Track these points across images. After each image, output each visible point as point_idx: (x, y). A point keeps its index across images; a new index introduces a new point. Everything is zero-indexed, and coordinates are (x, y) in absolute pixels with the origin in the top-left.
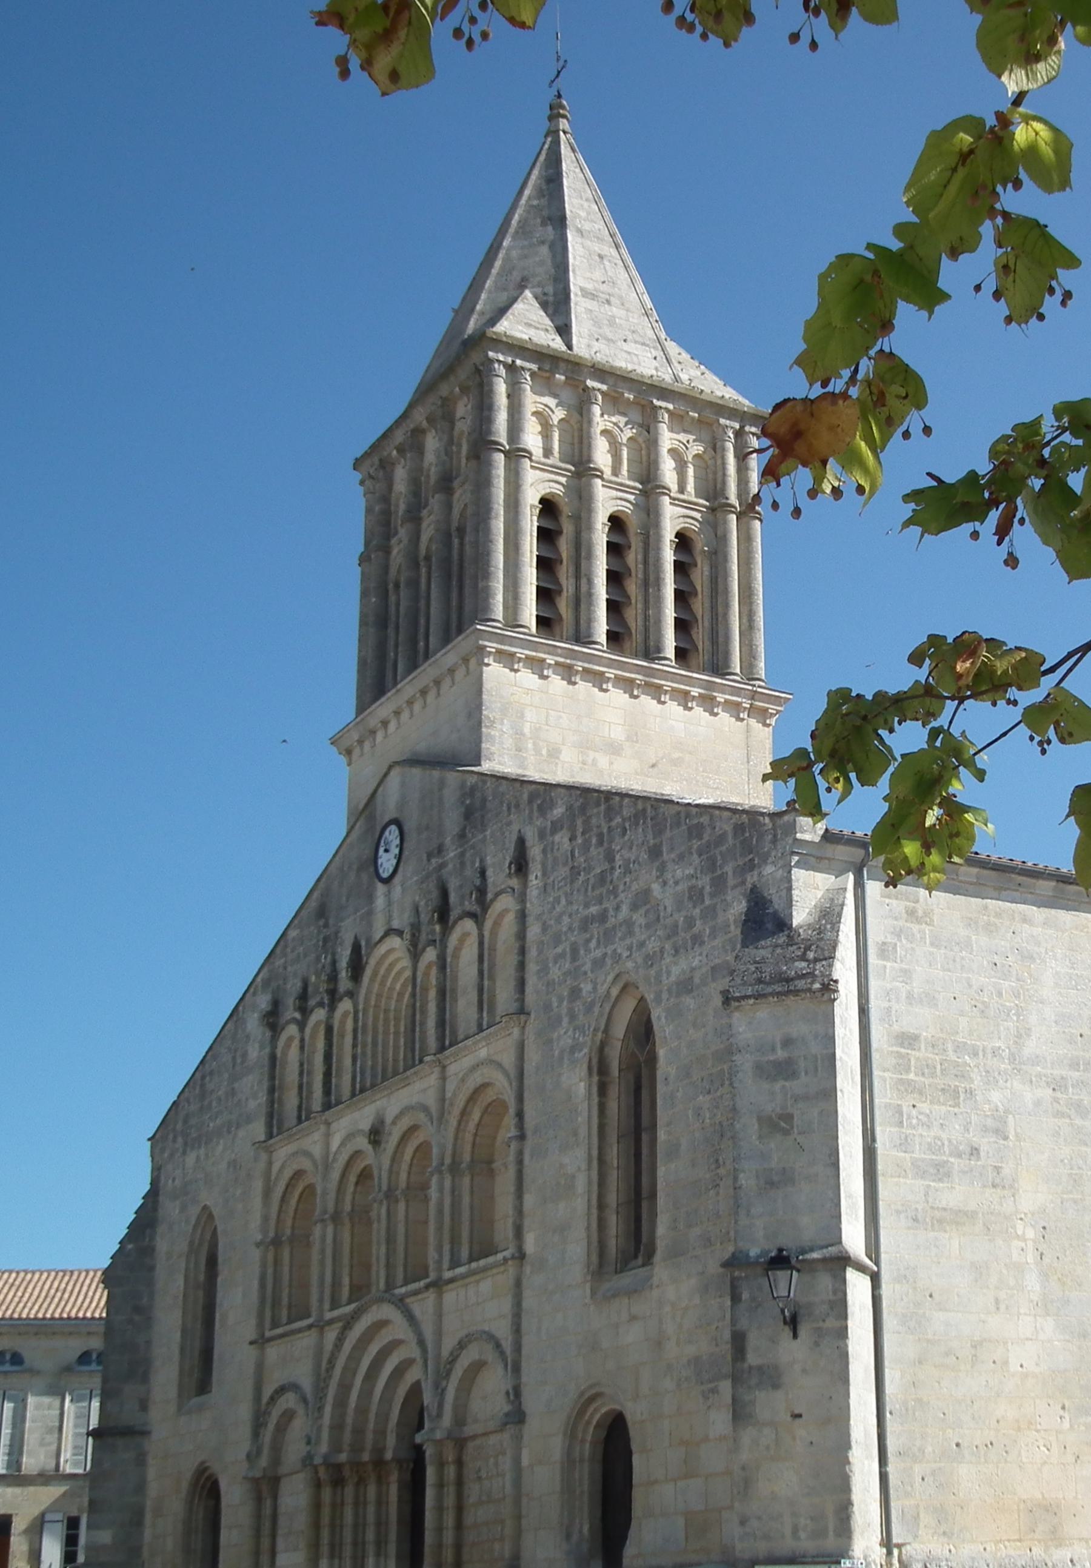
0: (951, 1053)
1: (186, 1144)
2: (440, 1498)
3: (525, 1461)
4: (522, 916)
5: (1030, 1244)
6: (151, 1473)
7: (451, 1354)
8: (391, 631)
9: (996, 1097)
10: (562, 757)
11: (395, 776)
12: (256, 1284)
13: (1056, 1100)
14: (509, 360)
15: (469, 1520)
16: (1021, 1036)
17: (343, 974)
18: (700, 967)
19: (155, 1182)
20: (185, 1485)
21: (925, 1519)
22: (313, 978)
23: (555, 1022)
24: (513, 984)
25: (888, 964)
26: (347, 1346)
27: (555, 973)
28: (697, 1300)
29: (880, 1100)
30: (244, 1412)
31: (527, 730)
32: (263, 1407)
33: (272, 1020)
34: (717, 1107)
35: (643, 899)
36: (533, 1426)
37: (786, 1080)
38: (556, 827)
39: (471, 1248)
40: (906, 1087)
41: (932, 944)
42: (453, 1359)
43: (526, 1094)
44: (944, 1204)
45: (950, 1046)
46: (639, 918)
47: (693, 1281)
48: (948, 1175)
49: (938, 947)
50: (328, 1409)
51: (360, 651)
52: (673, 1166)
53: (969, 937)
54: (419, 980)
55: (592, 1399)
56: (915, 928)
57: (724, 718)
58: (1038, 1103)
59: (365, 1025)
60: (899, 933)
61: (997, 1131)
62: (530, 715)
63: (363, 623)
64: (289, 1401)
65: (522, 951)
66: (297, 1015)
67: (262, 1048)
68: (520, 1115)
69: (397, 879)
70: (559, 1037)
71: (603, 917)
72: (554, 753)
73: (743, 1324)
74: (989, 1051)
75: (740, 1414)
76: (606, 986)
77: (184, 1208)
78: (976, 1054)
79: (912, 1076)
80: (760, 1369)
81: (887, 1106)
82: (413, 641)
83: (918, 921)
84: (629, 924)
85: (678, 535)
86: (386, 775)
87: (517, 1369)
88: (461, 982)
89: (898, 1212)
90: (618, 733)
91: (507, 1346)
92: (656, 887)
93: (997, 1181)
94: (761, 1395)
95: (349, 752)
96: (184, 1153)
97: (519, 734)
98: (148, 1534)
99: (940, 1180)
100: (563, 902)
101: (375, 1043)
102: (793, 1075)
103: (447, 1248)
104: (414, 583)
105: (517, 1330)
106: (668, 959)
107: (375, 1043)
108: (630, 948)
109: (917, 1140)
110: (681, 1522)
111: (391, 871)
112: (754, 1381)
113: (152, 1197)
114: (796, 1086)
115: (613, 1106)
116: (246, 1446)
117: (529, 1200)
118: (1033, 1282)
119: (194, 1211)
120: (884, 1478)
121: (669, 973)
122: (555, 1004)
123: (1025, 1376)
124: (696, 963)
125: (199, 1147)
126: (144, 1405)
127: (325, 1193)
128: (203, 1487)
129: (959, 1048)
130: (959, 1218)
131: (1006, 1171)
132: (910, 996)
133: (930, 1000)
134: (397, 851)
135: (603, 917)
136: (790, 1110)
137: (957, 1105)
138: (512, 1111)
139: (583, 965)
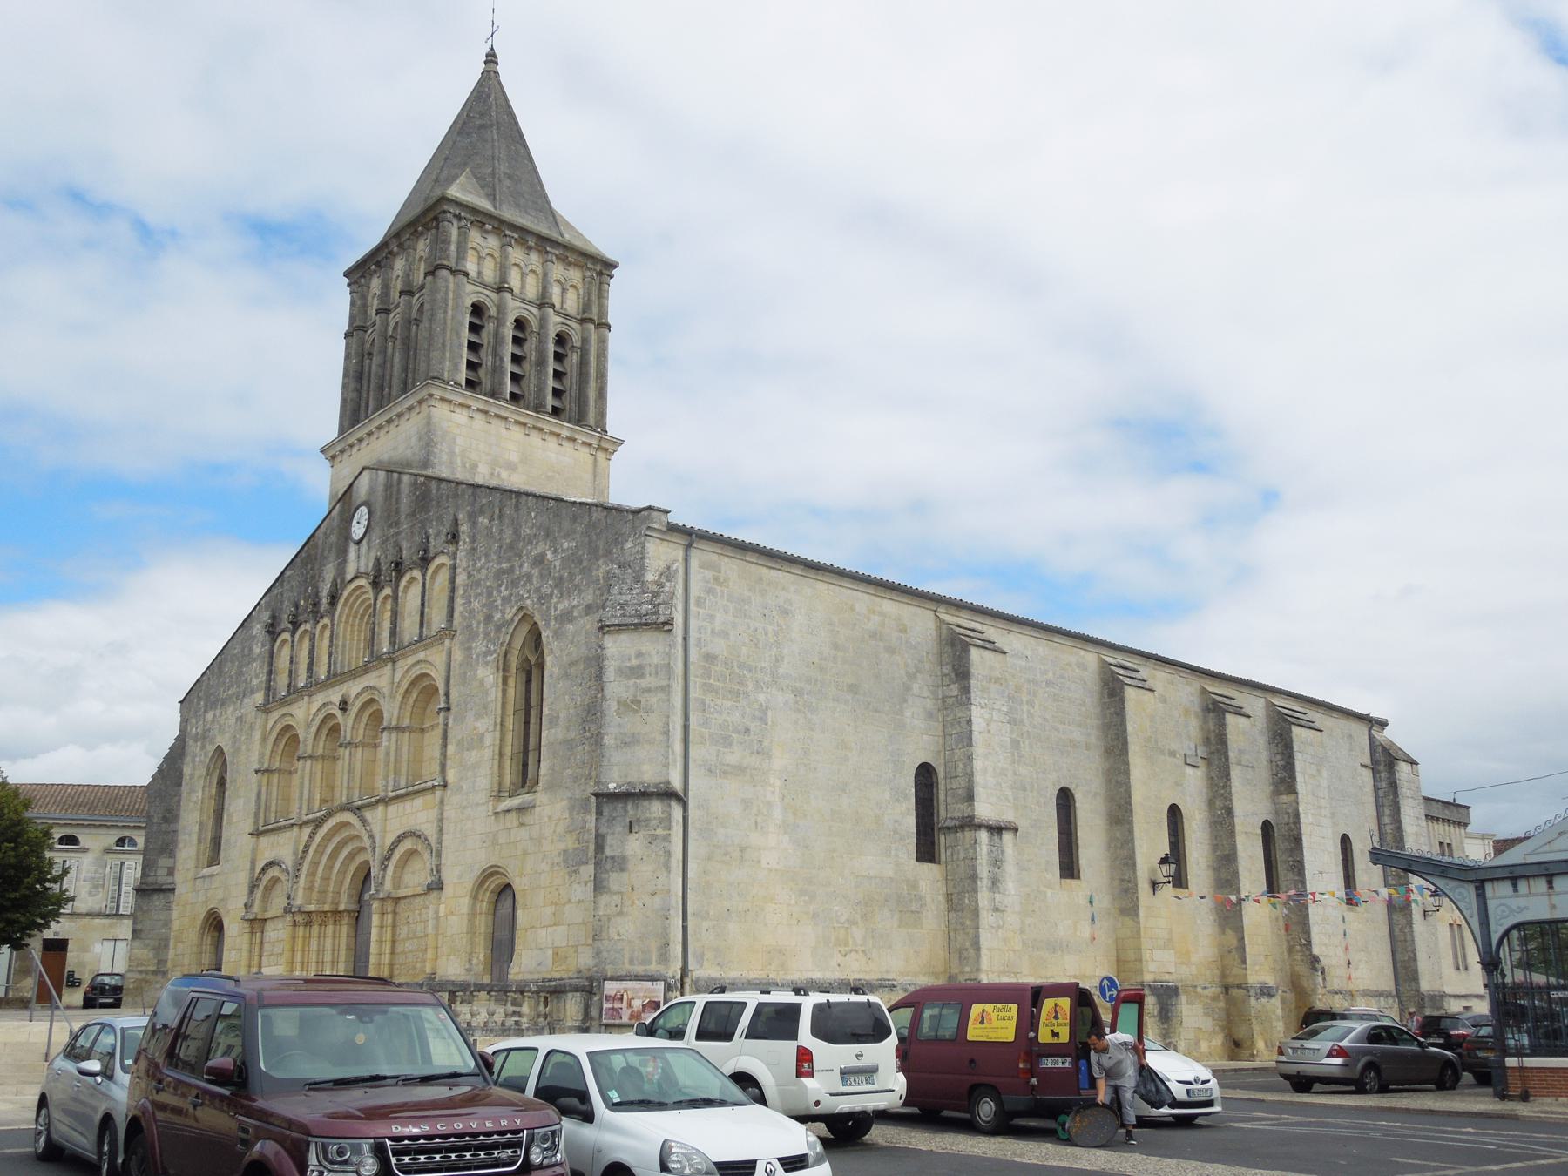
0: (736, 667)
1: (206, 706)
2: (380, 935)
3: (441, 914)
4: (454, 568)
5: (777, 789)
6: (175, 915)
7: (392, 844)
8: (365, 382)
9: (762, 697)
10: (479, 470)
11: (366, 476)
12: (254, 797)
13: (797, 702)
14: (457, 212)
15: (399, 948)
16: (778, 660)
17: (324, 601)
18: (578, 606)
19: (183, 731)
20: (199, 923)
21: (709, 955)
22: (302, 603)
23: (472, 636)
24: (445, 611)
25: (701, 611)
26: (318, 838)
27: (476, 605)
28: (566, 815)
29: (692, 695)
30: (243, 879)
31: (457, 451)
32: (256, 875)
33: (272, 631)
34: (586, 695)
35: (540, 560)
36: (448, 890)
37: (637, 678)
38: (482, 512)
39: (407, 779)
40: (708, 688)
41: (728, 600)
42: (392, 849)
43: (452, 682)
44: (727, 762)
45: (735, 664)
46: (535, 572)
47: (565, 803)
48: (731, 744)
49: (731, 602)
50: (303, 877)
51: (343, 393)
52: (553, 731)
53: (750, 597)
54: (378, 606)
55: (491, 875)
56: (718, 589)
57: (585, 451)
58: (786, 703)
59: (337, 634)
60: (710, 591)
61: (761, 719)
62: (460, 441)
63: (345, 375)
64: (274, 872)
65: (453, 590)
66: (290, 626)
67: (263, 646)
68: (447, 695)
69: (364, 542)
70: (477, 646)
71: (512, 570)
72: (474, 467)
73: (603, 830)
74: (758, 669)
75: (599, 887)
76: (511, 615)
77: (203, 747)
78: (750, 671)
79: (712, 681)
80: (613, 858)
81: (696, 699)
82: (381, 388)
83: (721, 584)
84: (529, 576)
85: (557, 335)
86: (361, 473)
87: (439, 855)
88: (407, 609)
89: (700, 765)
90: (514, 457)
91: (433, 840)
92: (549, 555)
93: (760, 750)
94: (614, 876)
95: (333, 458)
96: (205, 711)
97: (452, 453)
98: (171, 953)
99: (725, 747)
100: (483, 560)
101: (344, 646)
102: (642, 676)
103: (391, 777)
104: (384, 351)
105: (440, 831)
106: (555, 600)
107: (344, 646)
108: (529, 592)
109: (714, 721)
110: (550, 952)
111: (361, 535)
112: (608, 866)
113: (181, 742)
114: (643, 683)
115: (511, 692)
116: (244, 899)
117: (451, 749)
118: (777, 813)
119: (211, 749)
120: (685, 928)
121: (556, 609)
122: (474, 626)
123: (770, 870)
124: (575, 603)
125: (216, 708)
126: (171, 872)
127: (305, 740)
128: (212, 923)
129: (741, 666)
130: (740, 770)
131: (766, 743)
132: (713, 631)
133: (725, 634)
134: (366, 523)
135: (512, 570)
136: (638, 698)
137: (738, 701)
138: (442, 691)
139: (495, 601)
